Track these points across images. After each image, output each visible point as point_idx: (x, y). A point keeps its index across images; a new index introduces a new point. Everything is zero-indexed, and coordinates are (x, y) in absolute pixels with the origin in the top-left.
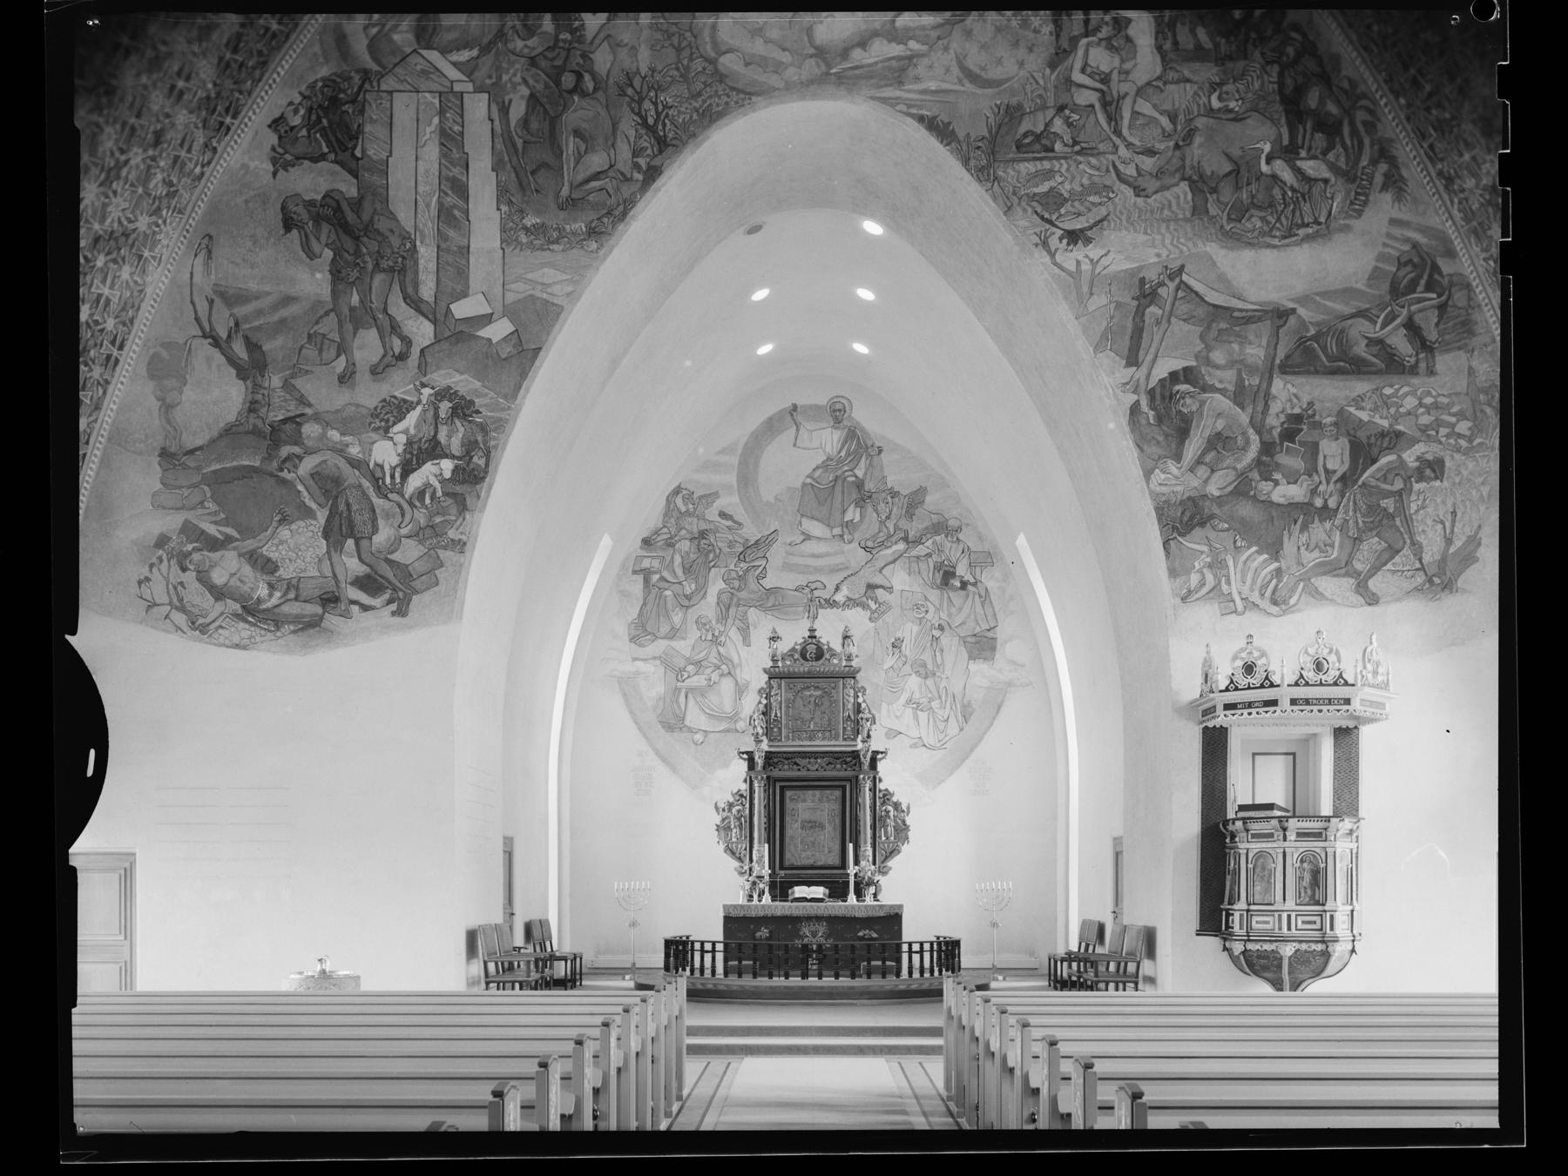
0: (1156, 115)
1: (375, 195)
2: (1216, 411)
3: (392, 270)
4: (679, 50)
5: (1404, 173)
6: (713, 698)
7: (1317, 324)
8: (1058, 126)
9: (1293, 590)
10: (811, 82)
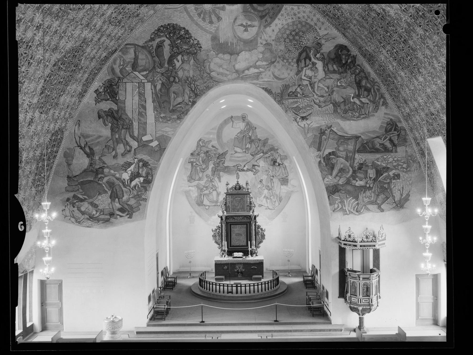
0: (324, 87)
1: (122, 109)
2: (341, 162)
3: (126, 128)
4: (200, 71)
5: (388, 101)
6: (211, 197)
7: (367, 140)
8: (299, 90)
9: (362, 208)
10: (235, 79)
